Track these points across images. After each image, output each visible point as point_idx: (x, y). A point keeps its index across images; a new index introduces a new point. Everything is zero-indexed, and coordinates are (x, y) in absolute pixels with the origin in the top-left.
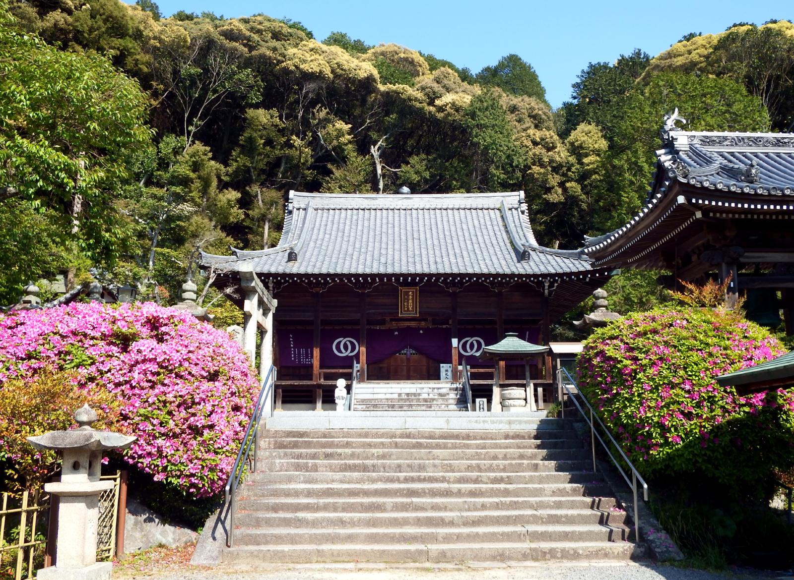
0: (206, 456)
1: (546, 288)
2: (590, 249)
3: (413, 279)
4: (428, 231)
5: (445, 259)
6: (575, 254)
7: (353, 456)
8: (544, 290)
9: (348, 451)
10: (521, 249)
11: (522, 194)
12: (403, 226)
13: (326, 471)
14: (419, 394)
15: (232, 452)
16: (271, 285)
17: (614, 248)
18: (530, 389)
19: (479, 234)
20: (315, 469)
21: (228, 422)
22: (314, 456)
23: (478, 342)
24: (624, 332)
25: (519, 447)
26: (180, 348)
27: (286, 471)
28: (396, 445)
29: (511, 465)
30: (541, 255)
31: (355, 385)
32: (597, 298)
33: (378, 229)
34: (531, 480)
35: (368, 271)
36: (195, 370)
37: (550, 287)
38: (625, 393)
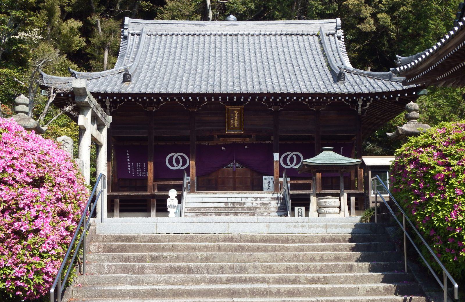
0: (31, 260)
1: (360, 106)
2: (402, 68)
3: (239, 99)
4: (252, 55)
5: (268, 80)
6: (387, 75)
7: (178, 259)
8: (357, 108)
9: (174, 254)
10: (338, 71)
12: (229, 50)
13: (152, 273)
14: (244, 203)
15: (58, 256)
16: (108, 105)
17: (421, 67)
18: (344, 198)
19: (299, 57)
20: (142, 271)
21: (54, 227)
22: (141, 259)
23: (297, 156)
24: (437, 140)
25: (335, 250)
26: (4, 155)
27: (114, 273)
28: (219, 249)
29: (327, 266)
30: (355, 76)
31: (185, 194)
32: (410, 111)
33: (206, 53)
34: (346, 280)
35: (197, 91)
36: (19, 176)
37: (363, 106)
38: (437, 198)
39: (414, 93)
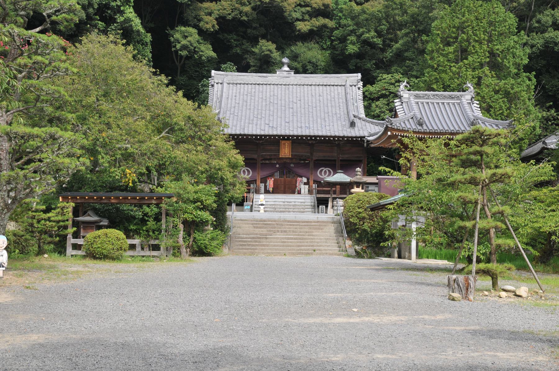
11: (359, 75)
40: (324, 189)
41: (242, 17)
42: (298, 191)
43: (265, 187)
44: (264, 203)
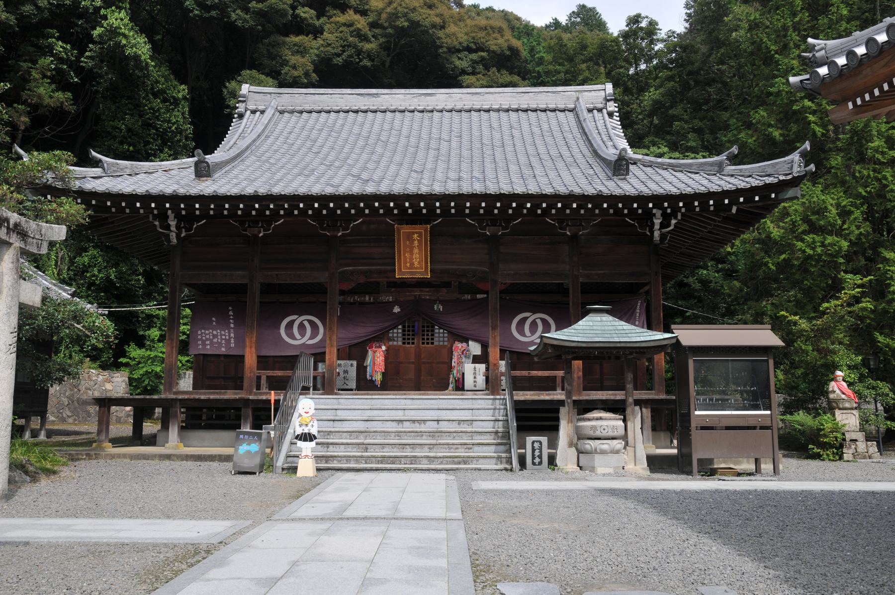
1: (657, 227)
8: (652, 232)
39: (773, 196)
40: (534, 373)
41: (361, 60)
42: (457, 381)
43: (361, 370)
44: (314, 431)
